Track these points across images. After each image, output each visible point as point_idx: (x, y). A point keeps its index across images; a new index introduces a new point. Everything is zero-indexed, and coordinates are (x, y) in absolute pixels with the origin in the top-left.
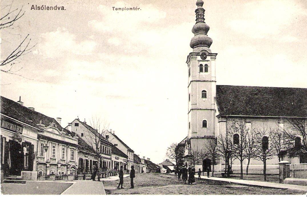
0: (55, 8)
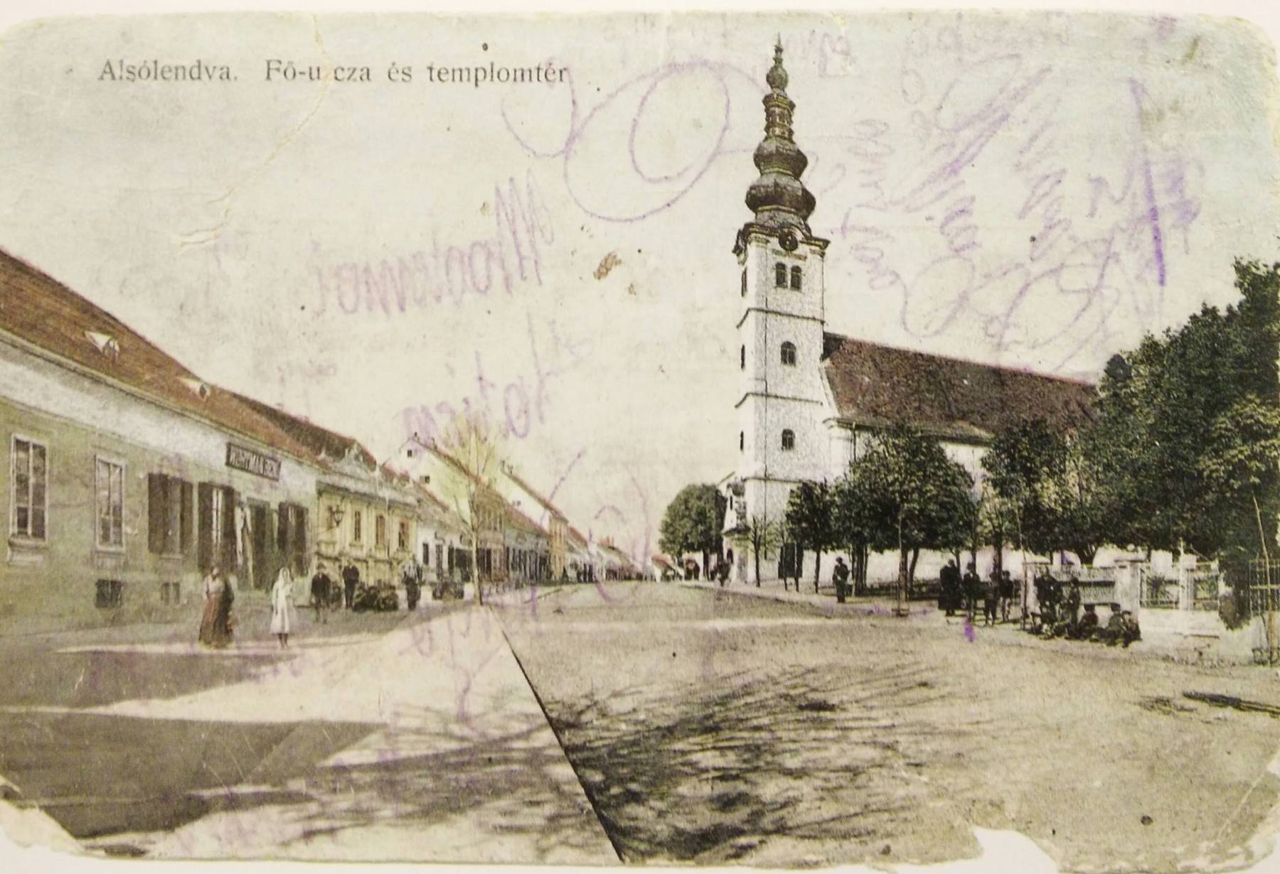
0: (195, 71)
